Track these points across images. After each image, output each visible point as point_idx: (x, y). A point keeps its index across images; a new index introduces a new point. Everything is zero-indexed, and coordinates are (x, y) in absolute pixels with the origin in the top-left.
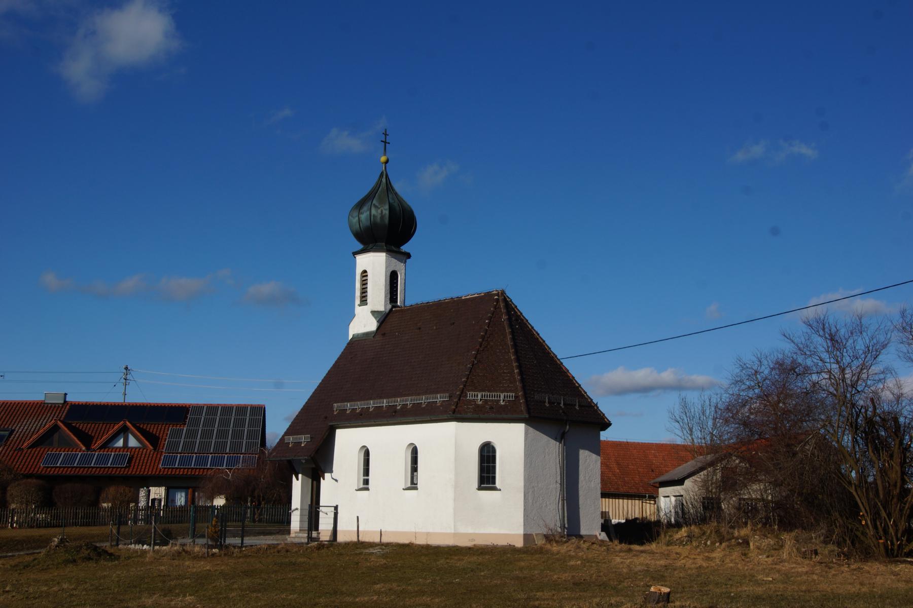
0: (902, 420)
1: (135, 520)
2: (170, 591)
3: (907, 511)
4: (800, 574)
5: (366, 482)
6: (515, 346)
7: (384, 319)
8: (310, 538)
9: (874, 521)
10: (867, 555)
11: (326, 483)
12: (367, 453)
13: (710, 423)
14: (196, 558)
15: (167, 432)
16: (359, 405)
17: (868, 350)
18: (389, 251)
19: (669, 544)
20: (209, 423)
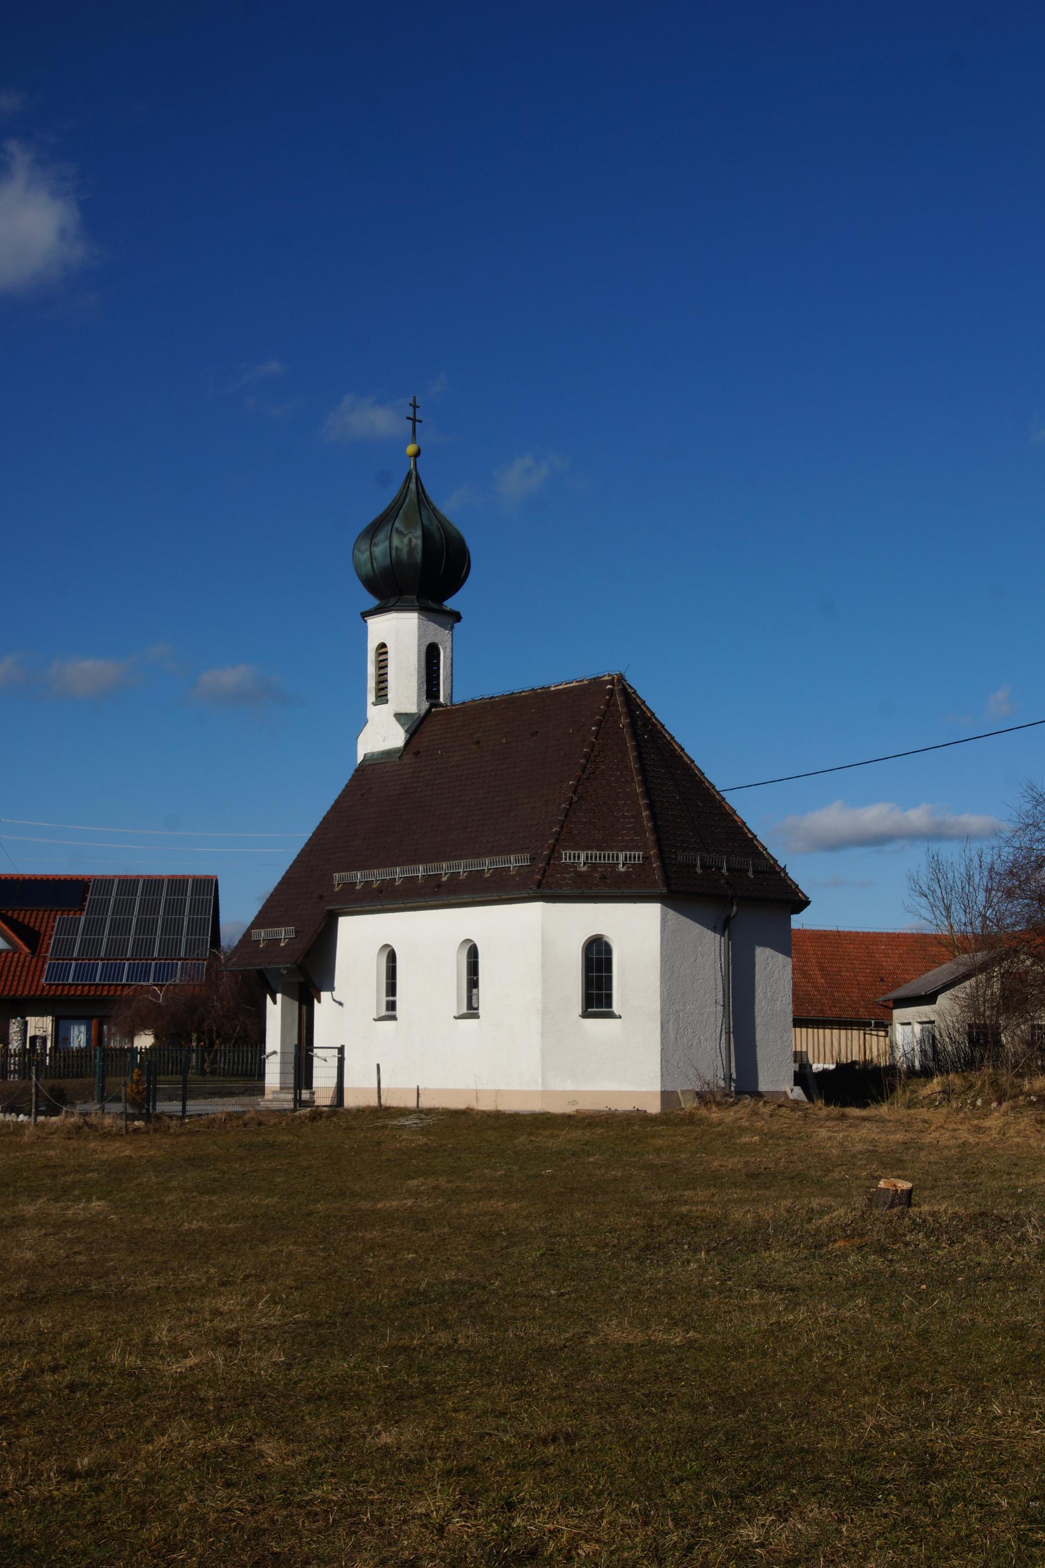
5: (392, 1006)
6: (643, 770)
7: (415, 727)
8: (298, 1102)
11: (323, 1009)
13: (981, 897)
14: (107, 1135)
15: (53, 925)
16: (377, 876)
18: (423, 610)
19: (910, 1105)
20: (124, 907)
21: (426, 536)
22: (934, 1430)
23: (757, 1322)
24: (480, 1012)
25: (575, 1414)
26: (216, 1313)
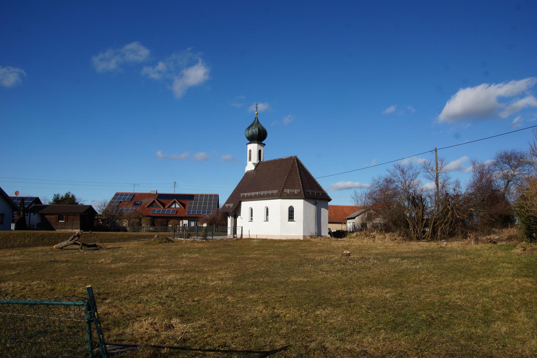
0: (423, 197)
1: (179, 231)
2: (191, 252)
3: (423, 226)
4: (390, 246)
5: (252, 219)
6: (300, 174)
7: (257, 166)
8: (234, 237)
9: (414, 229)
10: (411, 239)
11: (239, 219)
12: (252, 210)
13: (364, 199)
14: (198, 242)
15: (188, 203)
16: (249, 194)
17: (413, 175)
18: (258, 143)
19: (350, 238)
20: (201, 200)
21: (259, 129)
22: (352, 295)
23: (320, 277)
24: (268, 220)
25: (286, 293)
26: (219, 275)
